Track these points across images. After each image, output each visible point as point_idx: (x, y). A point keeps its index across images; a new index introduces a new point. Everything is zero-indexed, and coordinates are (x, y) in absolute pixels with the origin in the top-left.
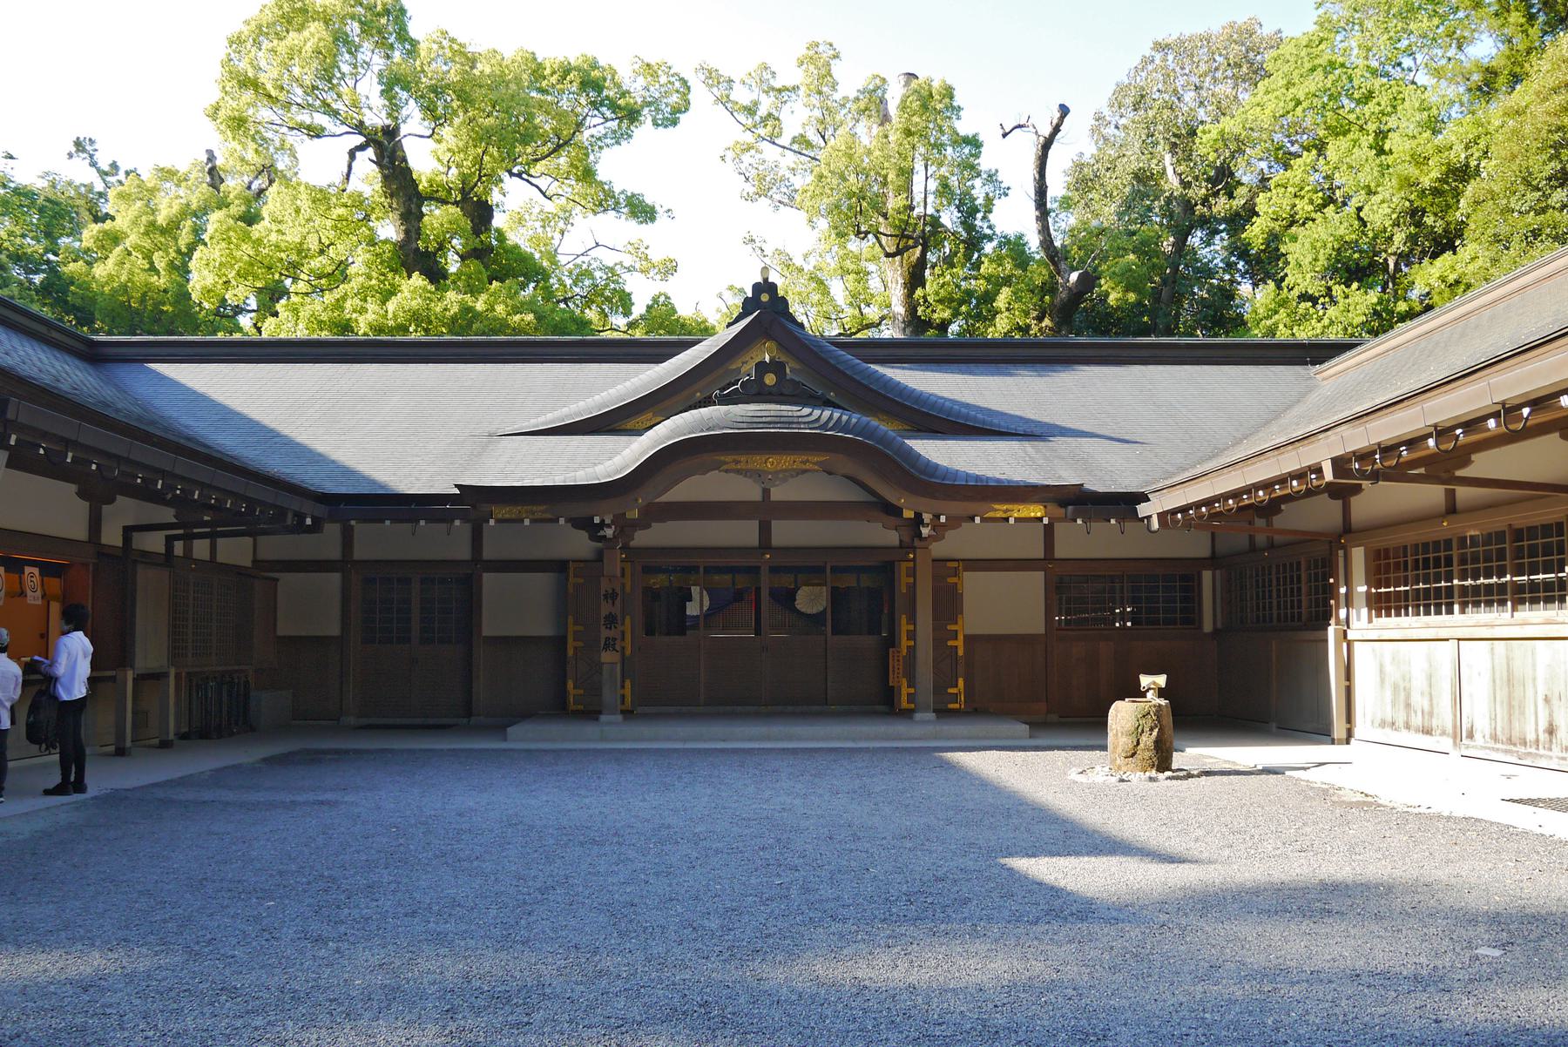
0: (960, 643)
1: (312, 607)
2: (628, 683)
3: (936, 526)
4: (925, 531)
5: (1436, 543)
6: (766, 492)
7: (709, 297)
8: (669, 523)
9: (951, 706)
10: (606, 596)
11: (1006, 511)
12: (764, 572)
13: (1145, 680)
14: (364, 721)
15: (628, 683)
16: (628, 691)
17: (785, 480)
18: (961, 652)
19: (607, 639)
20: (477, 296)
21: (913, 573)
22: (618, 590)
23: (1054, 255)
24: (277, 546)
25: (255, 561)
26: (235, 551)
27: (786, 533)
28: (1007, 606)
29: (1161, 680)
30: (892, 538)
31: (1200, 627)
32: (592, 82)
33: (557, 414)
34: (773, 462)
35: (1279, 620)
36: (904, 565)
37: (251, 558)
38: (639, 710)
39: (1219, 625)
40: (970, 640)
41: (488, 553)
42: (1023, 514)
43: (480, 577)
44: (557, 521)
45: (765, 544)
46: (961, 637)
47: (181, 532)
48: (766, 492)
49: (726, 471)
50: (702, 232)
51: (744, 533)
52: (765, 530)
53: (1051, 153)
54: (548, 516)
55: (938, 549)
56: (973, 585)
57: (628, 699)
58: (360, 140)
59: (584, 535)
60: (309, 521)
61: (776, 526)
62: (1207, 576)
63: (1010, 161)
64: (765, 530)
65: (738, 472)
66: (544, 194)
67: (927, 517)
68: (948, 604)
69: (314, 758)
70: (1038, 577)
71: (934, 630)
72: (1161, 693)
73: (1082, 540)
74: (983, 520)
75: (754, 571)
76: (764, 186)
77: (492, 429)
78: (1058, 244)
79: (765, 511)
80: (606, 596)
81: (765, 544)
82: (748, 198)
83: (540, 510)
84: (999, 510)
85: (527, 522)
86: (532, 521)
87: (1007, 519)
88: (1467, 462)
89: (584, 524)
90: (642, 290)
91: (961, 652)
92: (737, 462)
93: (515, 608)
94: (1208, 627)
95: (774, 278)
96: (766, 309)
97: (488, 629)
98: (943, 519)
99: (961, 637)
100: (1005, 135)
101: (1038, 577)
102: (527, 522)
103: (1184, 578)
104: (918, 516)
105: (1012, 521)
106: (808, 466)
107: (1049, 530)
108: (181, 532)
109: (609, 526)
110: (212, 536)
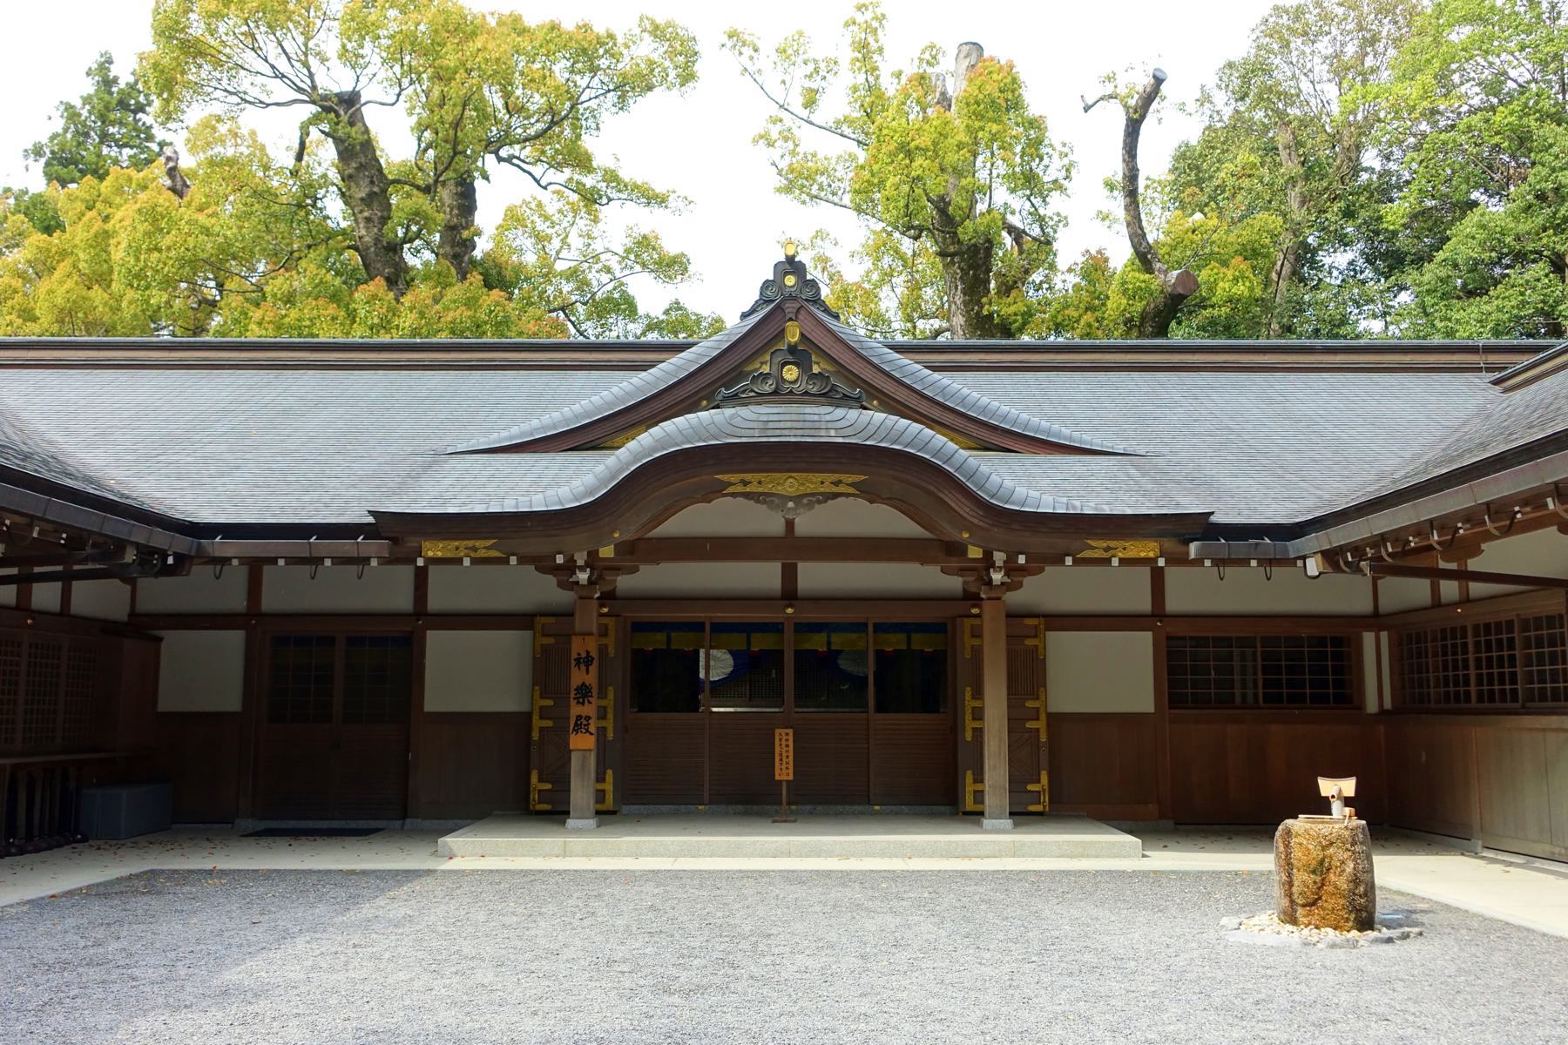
0: (1041, 725)
1: (206, 675)
2: (610, 774)
3: (1011, 569)
4: (997, 577)
5: (1498, 625)
6: (790, 525)
7: (724, 297)
8: (663, 566)
9: (1032, 808)
10: (578, 661)
11: (1107, 549)
12: (789, 634)
13: (1327, 787)
14: (262, 825)
15: (610, 774)
16: (608, 786)
17: (810, 506)
18: (1043, 738)
19: (579, 717)
20: (393, 253)
21: (977, 633)
22: (594, 654)
23: (1145, 257)
24: (159, 594)
25: (132, 614)
26: (97, 598)
27: (815, 576)
28: (1108, 676)
29: (1348, 786)
30: (954, 583)
31: (1361, 707)
32: (588, 51)
33: (525, 427)
34: (789, 484)
35: (1480, 699)
36: (968, 622)
37: (127, 610)
38: (625, 809)
39: (1388, 705)
40: (1056, 720)
41: (435, 603)
42: (1131, 554)
43: (424, 638)
44: (506, 561)
45: (789, 593)
46: (1043, 716)
47: (14, 571)
48: (790, 525)
49: (733, 495)
50: (710, 211)
51: (764, 576)
52: (789, 573)
53: (1145, 128)
54: (495, 554)
55: (1014, 598)
56: (1062, 646)
57: (610, 797)
58: (314, 109)
59: (551, 580)
60: (170, 560)
61: (803, 567)
62: (1368, 638)
63: (1086, 146)
64: (789, 573)
65: (747, 495)
66: (538, 182)
67: (999, 557)
68: (1027, 675)
69: (150, 882)
70: (1143, 642)
71: (1009, 707)
72: (1348, 802)
73: (1198, 590)
74: (1076, 562)
75: (776, 628)
76: (801, 181)
77: (439, 445)
78: (1150, 238)
79: (790, 548)
80: (578, 661)
81: (789, 593)
82: (779, 190)
83: (484, 547)
84: (1097, 548)
85: (467, 562)
86: (474, 561)
87: (1107, 561)
88: (1477, 551)
89: (544, 564)
90: (651, 296)
91: (1043, 738)
92: (745, 483)
93: (470, 675)
94: (1372, 706)
95: (804, 257)
96: (791, 296)
97: (432, 703)
98: (1022, 560)
99: (1043, 716)
100: (1087, 109)
101: (1143, 642)
102: (467, 562)
103: (1337, 642)
104: (988, 555)
105: (1115, 562)
106: (842, 489)
107: (1158, 577)
108: (14, 571)
109: (582, 569)
110: (67, 578)
